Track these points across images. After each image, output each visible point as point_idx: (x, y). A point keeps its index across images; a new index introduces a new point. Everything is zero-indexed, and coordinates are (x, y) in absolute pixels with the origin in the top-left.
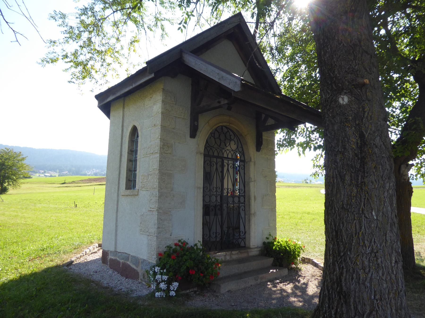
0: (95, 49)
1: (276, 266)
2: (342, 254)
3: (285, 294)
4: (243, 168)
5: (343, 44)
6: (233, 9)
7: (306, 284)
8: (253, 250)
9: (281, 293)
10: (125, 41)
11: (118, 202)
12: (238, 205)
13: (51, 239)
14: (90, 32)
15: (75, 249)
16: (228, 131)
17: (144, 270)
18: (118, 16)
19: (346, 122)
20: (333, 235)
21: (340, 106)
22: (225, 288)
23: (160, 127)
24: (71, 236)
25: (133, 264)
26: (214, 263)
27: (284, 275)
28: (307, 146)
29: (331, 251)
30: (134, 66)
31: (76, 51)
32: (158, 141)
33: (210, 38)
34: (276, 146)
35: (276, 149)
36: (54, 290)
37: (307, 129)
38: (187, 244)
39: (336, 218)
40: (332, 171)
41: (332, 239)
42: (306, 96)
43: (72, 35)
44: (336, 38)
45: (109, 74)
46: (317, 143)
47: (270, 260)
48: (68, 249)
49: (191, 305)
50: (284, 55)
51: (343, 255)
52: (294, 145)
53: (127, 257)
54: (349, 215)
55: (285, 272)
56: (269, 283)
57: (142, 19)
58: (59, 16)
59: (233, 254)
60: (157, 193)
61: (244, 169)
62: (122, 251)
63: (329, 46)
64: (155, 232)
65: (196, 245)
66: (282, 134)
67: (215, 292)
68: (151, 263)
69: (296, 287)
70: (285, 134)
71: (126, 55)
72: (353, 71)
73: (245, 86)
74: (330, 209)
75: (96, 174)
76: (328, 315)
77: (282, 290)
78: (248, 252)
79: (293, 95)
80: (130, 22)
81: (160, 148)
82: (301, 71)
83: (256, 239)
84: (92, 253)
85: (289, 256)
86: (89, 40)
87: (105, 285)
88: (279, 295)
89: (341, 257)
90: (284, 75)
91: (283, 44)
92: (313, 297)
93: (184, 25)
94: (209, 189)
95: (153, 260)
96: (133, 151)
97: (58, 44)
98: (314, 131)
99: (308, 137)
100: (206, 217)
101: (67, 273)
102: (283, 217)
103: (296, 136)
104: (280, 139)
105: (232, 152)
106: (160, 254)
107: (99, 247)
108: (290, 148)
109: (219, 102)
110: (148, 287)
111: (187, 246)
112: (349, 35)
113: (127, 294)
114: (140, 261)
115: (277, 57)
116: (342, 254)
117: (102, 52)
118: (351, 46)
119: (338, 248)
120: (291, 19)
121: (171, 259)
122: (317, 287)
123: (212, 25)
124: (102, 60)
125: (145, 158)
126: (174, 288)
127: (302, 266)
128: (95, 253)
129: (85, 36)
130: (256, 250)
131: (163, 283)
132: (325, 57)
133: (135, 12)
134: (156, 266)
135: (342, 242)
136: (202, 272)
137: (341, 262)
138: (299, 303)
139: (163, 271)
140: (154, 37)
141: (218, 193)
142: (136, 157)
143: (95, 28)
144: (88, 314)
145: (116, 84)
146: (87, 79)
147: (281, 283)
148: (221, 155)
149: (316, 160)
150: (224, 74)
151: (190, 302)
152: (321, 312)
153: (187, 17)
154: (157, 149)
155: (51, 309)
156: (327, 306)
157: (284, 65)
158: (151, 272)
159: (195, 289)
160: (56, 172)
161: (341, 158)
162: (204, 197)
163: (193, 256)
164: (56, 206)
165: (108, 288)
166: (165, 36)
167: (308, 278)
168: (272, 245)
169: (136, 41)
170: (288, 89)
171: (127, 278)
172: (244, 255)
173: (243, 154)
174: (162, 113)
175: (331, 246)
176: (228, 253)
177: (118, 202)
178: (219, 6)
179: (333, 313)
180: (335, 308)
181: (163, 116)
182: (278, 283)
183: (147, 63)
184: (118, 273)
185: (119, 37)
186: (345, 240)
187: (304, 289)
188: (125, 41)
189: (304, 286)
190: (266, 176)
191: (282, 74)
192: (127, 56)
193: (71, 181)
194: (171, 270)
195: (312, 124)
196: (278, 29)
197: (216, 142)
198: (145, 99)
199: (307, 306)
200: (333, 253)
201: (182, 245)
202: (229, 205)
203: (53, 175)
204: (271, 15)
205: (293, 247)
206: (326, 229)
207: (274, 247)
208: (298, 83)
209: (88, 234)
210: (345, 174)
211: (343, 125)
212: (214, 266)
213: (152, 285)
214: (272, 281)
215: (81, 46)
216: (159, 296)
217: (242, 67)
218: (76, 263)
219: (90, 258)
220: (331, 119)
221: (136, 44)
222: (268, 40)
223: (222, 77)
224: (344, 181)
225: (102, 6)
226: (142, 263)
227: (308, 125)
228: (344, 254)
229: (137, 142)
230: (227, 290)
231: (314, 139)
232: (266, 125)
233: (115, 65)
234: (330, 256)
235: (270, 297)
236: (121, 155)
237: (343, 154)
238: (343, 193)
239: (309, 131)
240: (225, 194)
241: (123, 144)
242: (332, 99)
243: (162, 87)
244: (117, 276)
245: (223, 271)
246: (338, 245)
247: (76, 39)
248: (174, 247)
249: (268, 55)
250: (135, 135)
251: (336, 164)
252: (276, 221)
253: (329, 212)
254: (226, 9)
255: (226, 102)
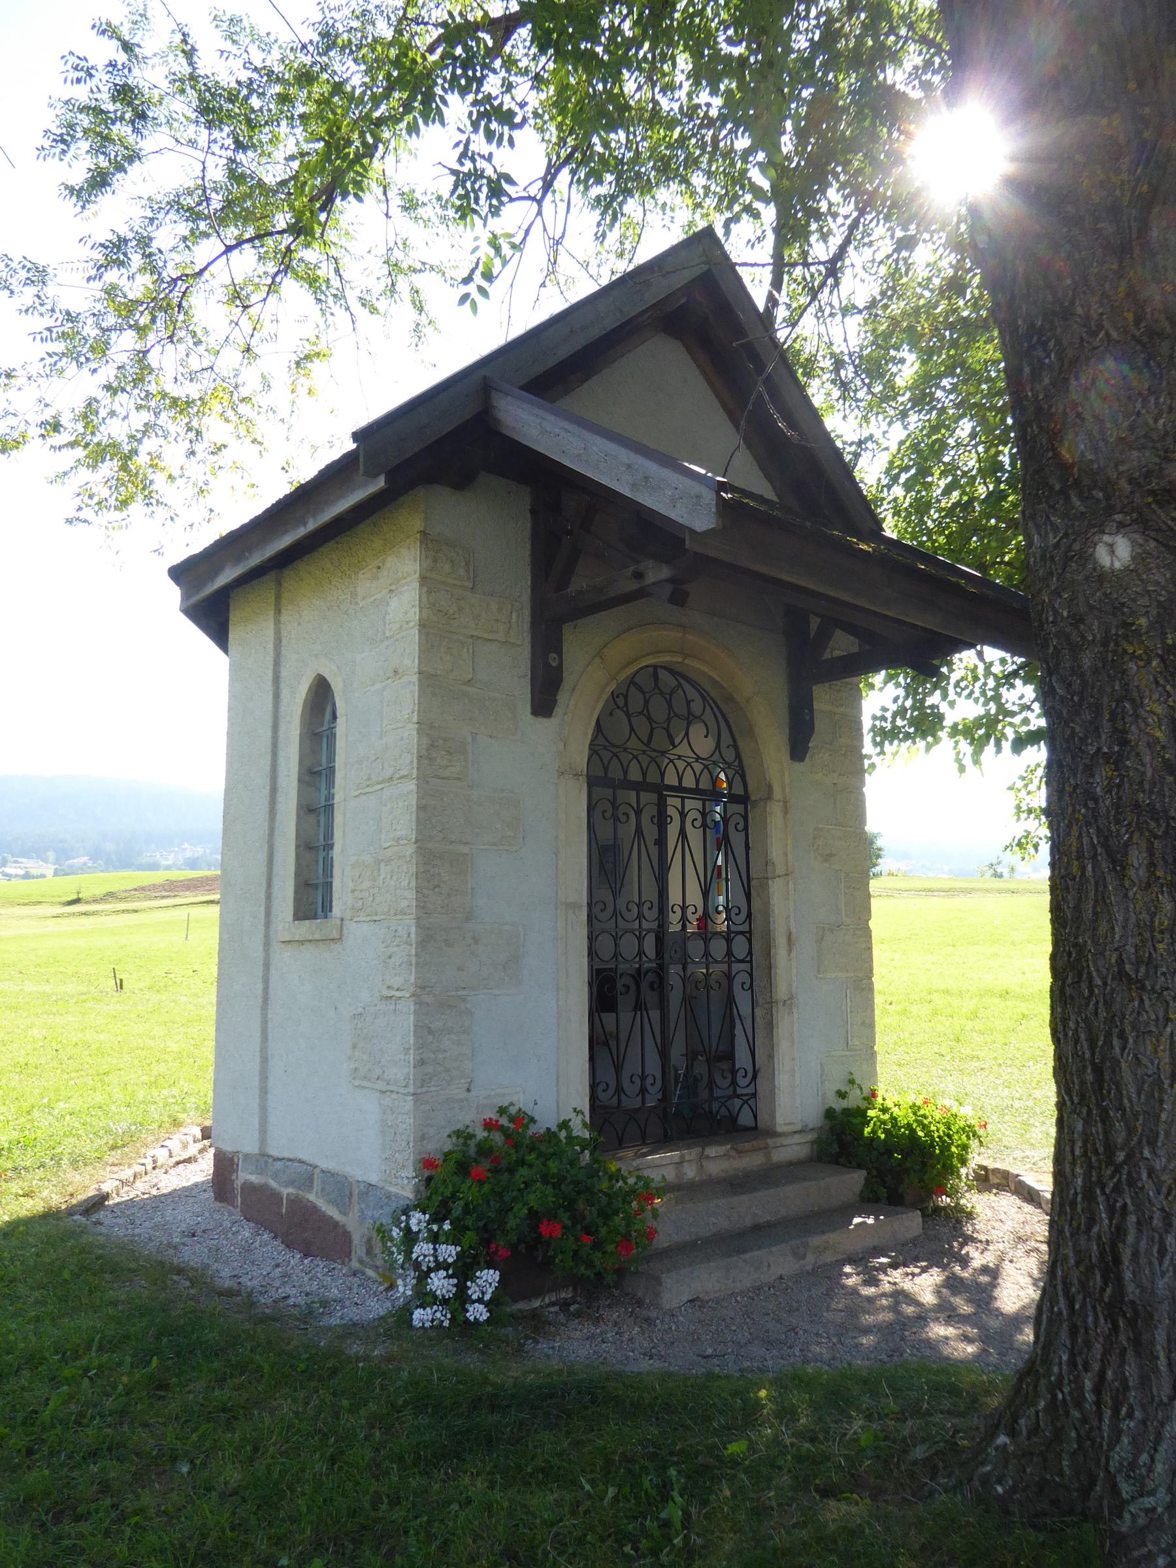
0: (164, 395)
1: (877, 1200)
2: (1121, 1156)
3: (910, 1310)
4: (740, 827)
5: (1107, 333)
6: (683, 216)
7: (993, 1273)
8: (785, 1141)
9: (894, 1308)
10: (274, 360)
11: (267, 965)
12: (725, 967)
13: (28, 1113)
14: (141, 331)
15: (114, 1148)
16: (680, 685)
17: (369, 1223)
18: (246, 262)
19: (1126, 637)
20: (1083, 1083)
21: (1102, 577)
22: (678, 1288)
23: (415, 678)
24: (99, 1098)
25: (329, 1202)
26: (633, 1191)
27: (910, 1236)
28: (988, 736)
29: (1079, 1144)
30: (315, 448)
31: (91, 406)
32: (410, 733)
33: (596, 332)
34: (867, 739)
35: (868, 748)
36: (37, 1302)
37: (988, 667)
38: (532, 1120)
39: (1096, 1014)
40: (1075, 831)
41: (1082, 1097)
42: (981, 539)
43: (75, 343)
44: (1079, 311)
45: (220, 485)
46: (1026, 721)
47: (855, 1180)
48: (87, 1147)
49: (548, 1356)
50: (890, 386)
51: (1124, 1162)
52: (940, 733)
53: (307, 1175)
54: (1147, 1002)
55: (911, 1223)
56: (848, 1269)
57: (337, 271)
58: (24, 274)
59: (708, 1157)
60: (413, 930)
61: (746, 828)
62: (286, 1155)
63: (1052, 344)
64: (407, 1078)
65: (564, 1125)
66: (892, 691)
67: (640, 1303)
68: (396, 1195)
69: (953, 1284)
70: (901, 692)
71: (283, 412)
72: (1146, 436)
73: (735, 510)
74: (1069, 981)
75: (192, 864)
76: (1070, 1393)
77: (900, 1296)
78: (766, 1148)
79: (930, 538)
80: (289, 285)
81: (420, 758)
82: (958, 445)
83: (795, 1098)
84: (178, 1163)
85: (924, 1164)
86: (140, 361)
87: (228, 1284)
88: (889, 1316)
89: (1117, 1170)
90: (891, 463)
91: (883, 342)
92: (1016, 1321)
93: (485, 284)
94: (610, 909)
95: (405, 1187)
96: (317, 773)
97: (20, 381)
98: (1015, 674)
99: (992, 698)
100: (604, 1015)
101: (84, 1239)
102: (904, 1012)
103: (945, 696)
104: (885, 709)
105: (698, 767)
106: (428, 1163)
107: (204, 1138)
108: (921, 744)
109: (639, 575)
110: (387, 1290)
111: (533, 1129)
112: (1128, 295)
113: (308, 1315)
114: (356, 1192)
115: (860, 395)
116: (1121, 1156)
117: (189, 403)
118: (1138, 341)
119: (1106, 1133)
120: (906, 244)
121: (468, 1182)
122: (1035, 1283)
123: (604, 282)
124: (192, 435)
125: (363, 797)
126: (483, 1293)
127: (976, 1201)
128: (188, 1161)
129: (124, 343)
130: (797, 1139)
131: (442, 1273)
132: (1038, 387)
133: (307, 245)
134: (415, 1207)
135: (1121, 1108)
136: (587, 1231)
137: (1117, 1189)
138: (962, 1345)
139: (440, 1228)
140: (388, 337)
141: (645, 925)
142: (330, 797)
143: (160, 315)
144: (162, 1393)
145: (246, 520)
146: (137, 508)
147: (894, 1266)
148: (653, 777)
149: (1026, 786)
150: (652, 467)
151: (543, 1346)
152: (1043, 1381)
153: (492, 252)
154: (407, 762)
155: (26, 1373)
156: (1065, 1358)
157: (890, 424)
158: (395, 1232)
159: (563, 1295)
160: (45, 860)
161: (1110, 779)
162: (591, 939)
163: (553, 1166)
164: (48, 988)
165: (238, 1293)
166: (428, 331)
167: (1001, 1246)
168: (858, 1120)
169: (318, 354)
170: (909, 514)
171: (306, 1256)
172: (752, 1161)
173: (739, 771)
174: (423, 625)
175: (1079, 1126)
176: (691, 1154)
177: (267, 965)
178: (626, 209)
179: (1088, 1385)
180: (1096, 1367)
181: (427, 634)
182: (883, 1269)
183: (356, 436)
184: (275, 1237)
185: (253, 343)
186: (1130, 1101)
187: (982, 1290)
188: (274, 360)
189: (984, 1279)
190: (831, 855)
191: (883, 460)
192: (287, 417)
193: (100, 891)
194: (469, 1222)
195: (1007, 652)
196: (859, 284)
197: (632, 730)
198: (356, 574)
199: (994, 1357)
200: (1085, 1154)
201: (512, 1126)
202: (691, 968)
203: (34, 872)
204: (830, 232)
205: (942, 1128)
206: (1059, 1057)
207: (867, 1130)
208: (947, 491)
209: (165, 1092)
210: (1127, 845)
211: (1115, 652)
212: (634, 1204)
213: (400, 1282)
214: (859, 1260)
215: (108, 387)
216: (428, 1324)
217: (724, 435)
218: (117, 1200)
219: (172, 1181)
220: (1068, 629)
221: (316, 366)
222: (822, 329)
223: (646, 478)
224: (1124, 868)
225: (183, 228)
226: (363, 1195)
227: (992, 654)
228: (1129, 1157)
229: (332, 738)
230: (685, 1299)
231: (1015, 708)
232: (827, 655)
233: (240, 451)
234: (1073, 1163)
235: (851, 1324)
236: (274, 790)
237: (1116, 763)
238: (1120, 918)
239: (995, 675)
240: (674, 927)
241: (280, 745)
242: (1069, 549)
243: (418, 524)
244: (269, 1248)
245: (670, 1222)
246: (1103, 1122)
247: (88, 360)
248: (481, 1134)
249: (828, 385)
250: (324, 710)
251: (1091, 804)
252: (872, 1026)
253: (1068, 991)
254: (654, 217)
255: (665, 572)
